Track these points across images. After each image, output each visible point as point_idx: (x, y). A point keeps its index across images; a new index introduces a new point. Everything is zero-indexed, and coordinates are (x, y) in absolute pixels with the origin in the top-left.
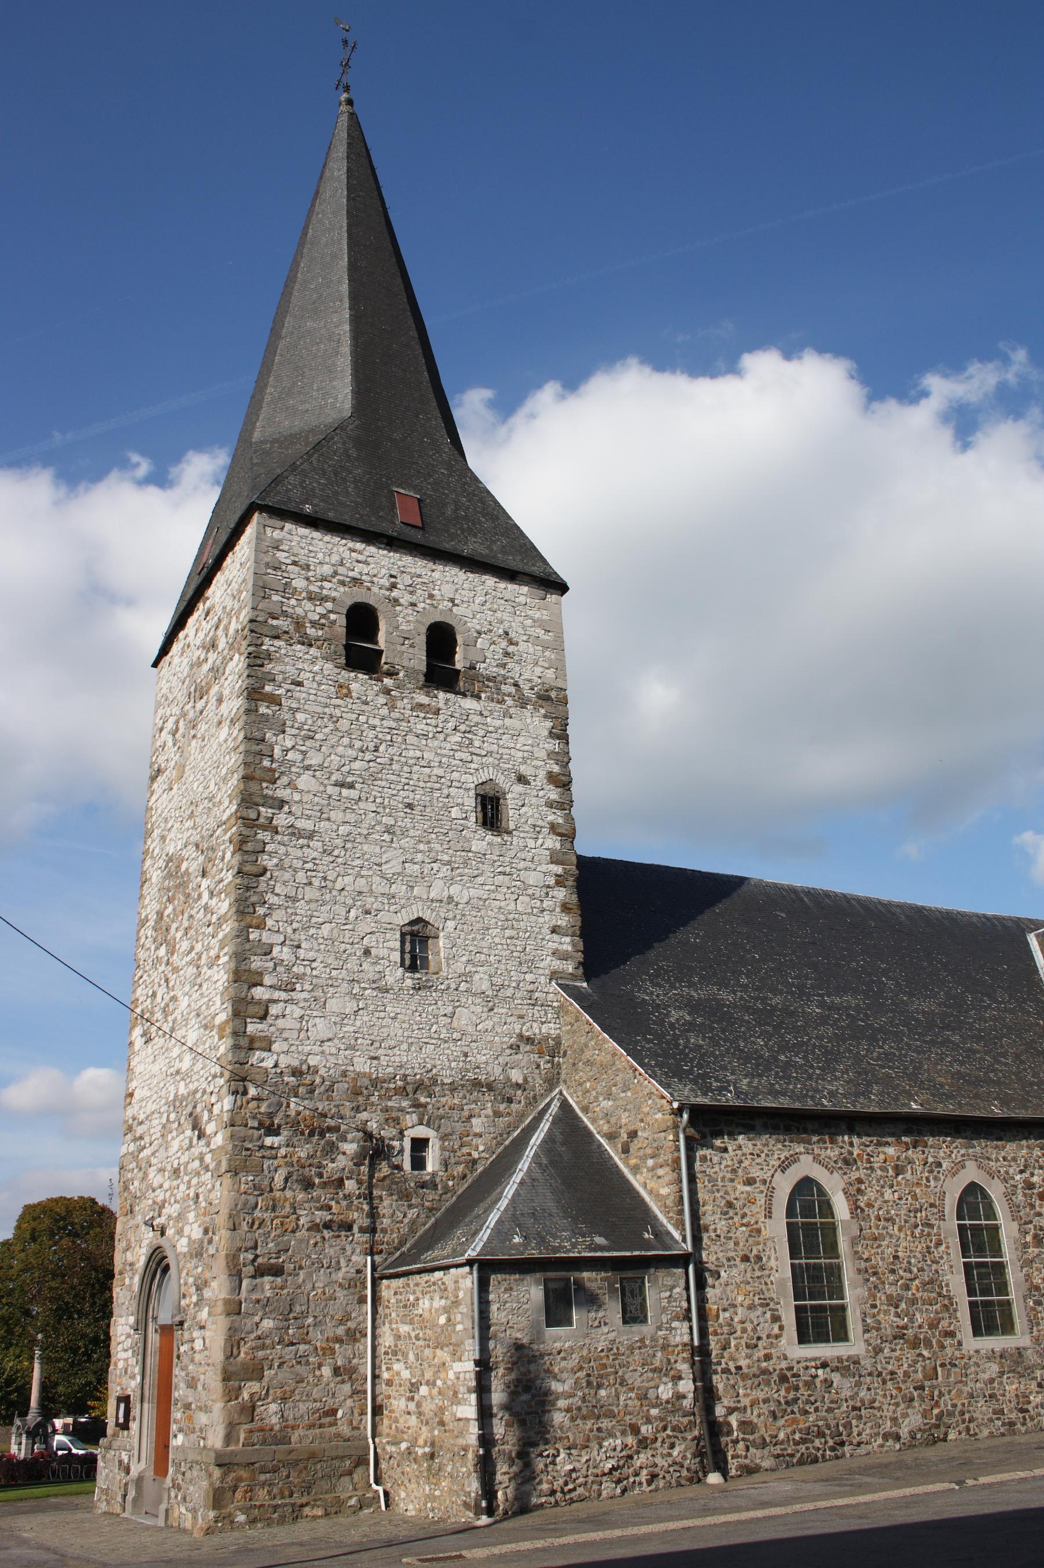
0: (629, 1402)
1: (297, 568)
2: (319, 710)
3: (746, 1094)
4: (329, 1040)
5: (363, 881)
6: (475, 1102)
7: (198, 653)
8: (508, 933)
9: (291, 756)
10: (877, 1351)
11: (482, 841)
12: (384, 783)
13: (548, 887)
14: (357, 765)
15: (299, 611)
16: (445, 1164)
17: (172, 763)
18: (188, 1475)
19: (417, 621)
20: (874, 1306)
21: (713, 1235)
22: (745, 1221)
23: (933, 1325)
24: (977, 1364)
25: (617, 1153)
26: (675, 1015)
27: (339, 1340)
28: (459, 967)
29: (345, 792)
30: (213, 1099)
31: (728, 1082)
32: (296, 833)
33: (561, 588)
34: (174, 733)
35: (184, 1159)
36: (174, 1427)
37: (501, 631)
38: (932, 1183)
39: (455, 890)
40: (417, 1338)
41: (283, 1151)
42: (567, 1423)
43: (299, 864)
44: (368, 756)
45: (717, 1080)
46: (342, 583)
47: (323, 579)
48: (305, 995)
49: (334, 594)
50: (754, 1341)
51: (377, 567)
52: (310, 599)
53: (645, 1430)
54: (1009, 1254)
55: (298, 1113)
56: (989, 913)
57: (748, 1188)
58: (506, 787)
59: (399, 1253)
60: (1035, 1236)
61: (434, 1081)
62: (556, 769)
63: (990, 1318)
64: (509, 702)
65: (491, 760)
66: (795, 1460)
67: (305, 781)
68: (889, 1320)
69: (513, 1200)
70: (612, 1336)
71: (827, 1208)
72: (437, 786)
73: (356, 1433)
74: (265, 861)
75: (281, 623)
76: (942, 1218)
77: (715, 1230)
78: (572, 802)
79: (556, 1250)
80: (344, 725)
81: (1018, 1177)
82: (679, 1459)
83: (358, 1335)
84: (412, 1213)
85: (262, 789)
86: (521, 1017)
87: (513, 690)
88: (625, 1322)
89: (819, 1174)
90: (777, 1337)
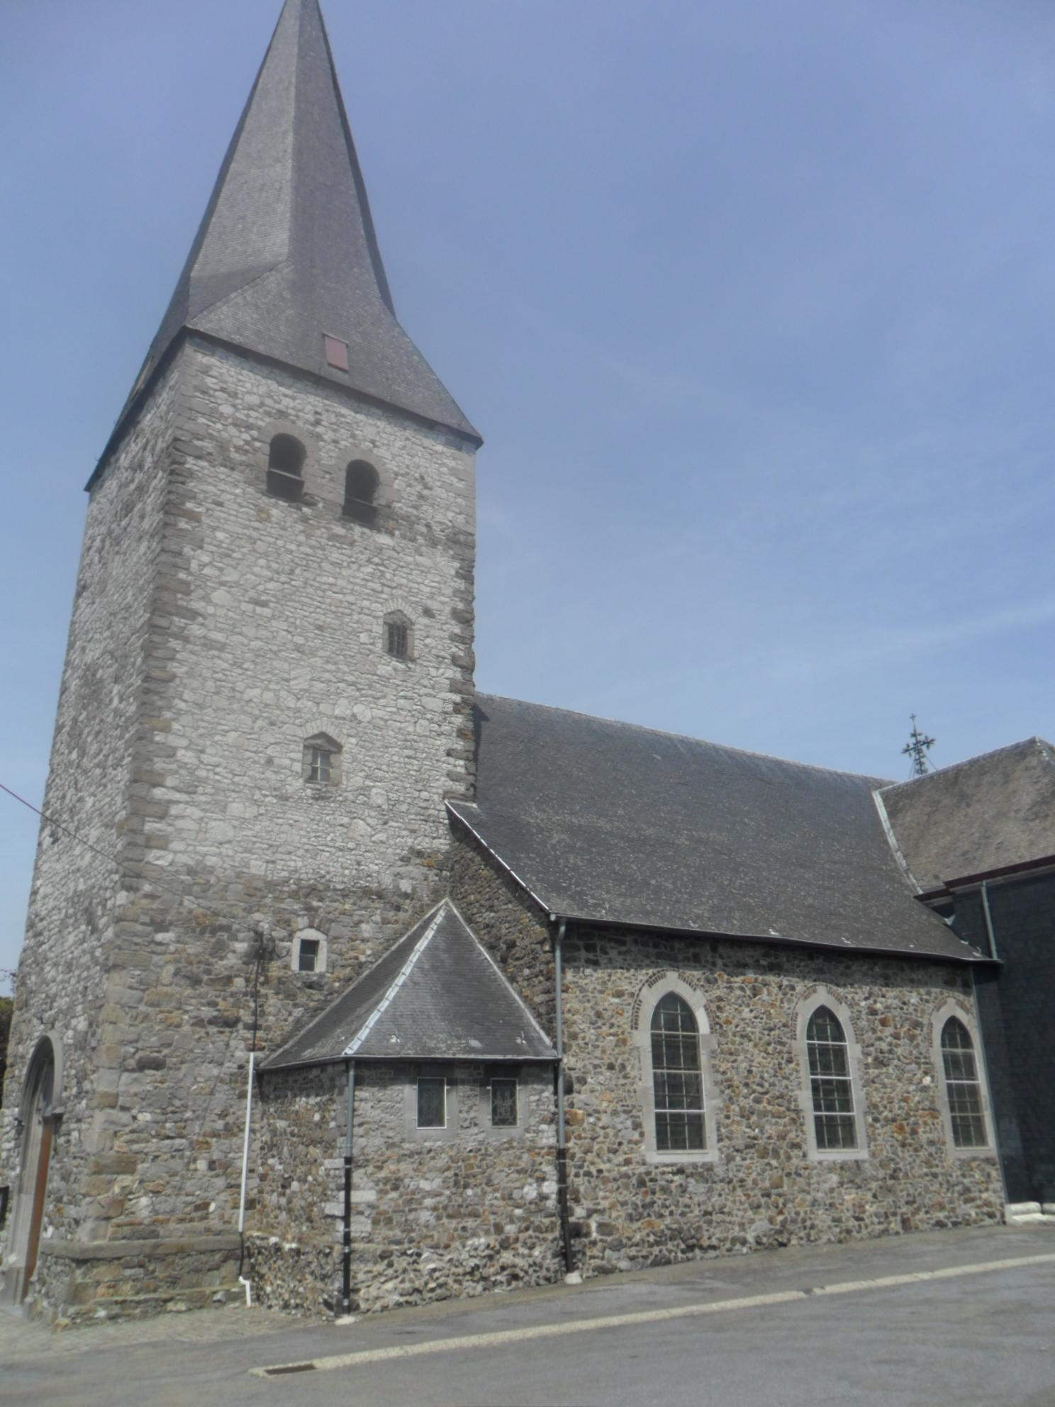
0: (495, 1202)
1: (225, 395)
2: (240, 530)
3: (620, 912)
4: (229, 842)
5: (271, 694)
6: (365, 908)
7: (126, 474)
8: (407, 752)
9: (207, 571)
10: (730, 1159)
11: (388, 666)
12: (296, 605)
13: (446, 713)
14: (271, 585)
15: (224, 435)
16: (332, 965)
17: (97, 579)
18: (53, 1268)
19: (338, 458)
20: (728, 1117)
21: (582, 1043)
22: (612, 1031)
23: (782, 1137)
24: (819, 1175)
25: (495, 961)
26: (556, 837)
27: (215, 1134)
28: (358, 780)
29: (259, 609)
30: (108, 894)
31: (604, 900)
32: (208, 644)
33: (477, 442)
34: (100, 551)
35: (76, 953)
36: (45, 1219)
37: (417, 475)
38: (786, 1005)
39: (358, 709)
40: (293, 1135)
41: (172, 948)
42: (433, 1221)
43: (209, 675)
44: (283, 578)
45: (593, 897)
46: (268, 414)
47: (251, 408)
48: (203, 798)
49: (260, 423)
50: (616, 1146)
51: (303, 408)
52: (235, 425)
53: (510, 1229)
54: (854, 1075)
55: (190, 912)
56: (840, 771)
57: (616, 1000)
58: (413, 617)
59: (281, 1050)
60: (876, 1059)
61: (327, 888)
62: (461, 606)
63: (834, 1132)
64: (420, 540)
65: (400, 592)
66: (649, 1261)
67: (220, 595)
68: (741, 1131)
69: (394, 1002)
70: (481, 1137)
71: (691, 1022)
72: (348, 611)
73: (228, 1227)
74: (174, 668)
75: (208, 445)
76: (794, 1037)
77: (584, 1039)
78: (473, 637)
79: (431, 1050)
80: (260, 546)
81: (863, 1004)
82: (538, 1261)
83: (235, 1130)
84: (298, 1012)
85: (176, 600)
86: (413, 831)
87: (424, 530)
88: (495, 1123)
89: (684, 990)
90: (637, 1143)
